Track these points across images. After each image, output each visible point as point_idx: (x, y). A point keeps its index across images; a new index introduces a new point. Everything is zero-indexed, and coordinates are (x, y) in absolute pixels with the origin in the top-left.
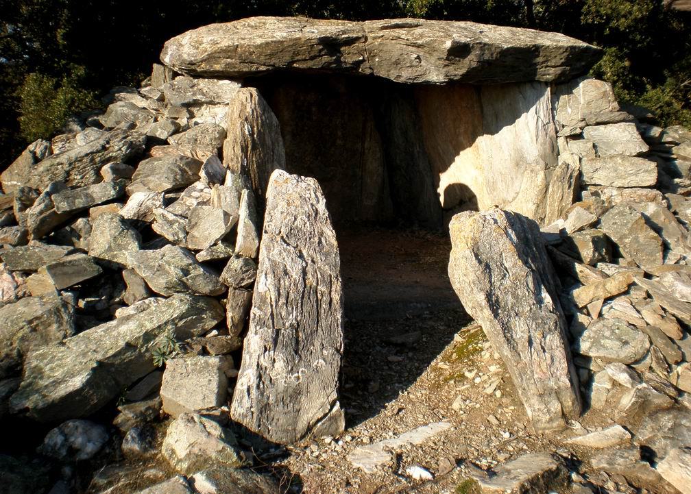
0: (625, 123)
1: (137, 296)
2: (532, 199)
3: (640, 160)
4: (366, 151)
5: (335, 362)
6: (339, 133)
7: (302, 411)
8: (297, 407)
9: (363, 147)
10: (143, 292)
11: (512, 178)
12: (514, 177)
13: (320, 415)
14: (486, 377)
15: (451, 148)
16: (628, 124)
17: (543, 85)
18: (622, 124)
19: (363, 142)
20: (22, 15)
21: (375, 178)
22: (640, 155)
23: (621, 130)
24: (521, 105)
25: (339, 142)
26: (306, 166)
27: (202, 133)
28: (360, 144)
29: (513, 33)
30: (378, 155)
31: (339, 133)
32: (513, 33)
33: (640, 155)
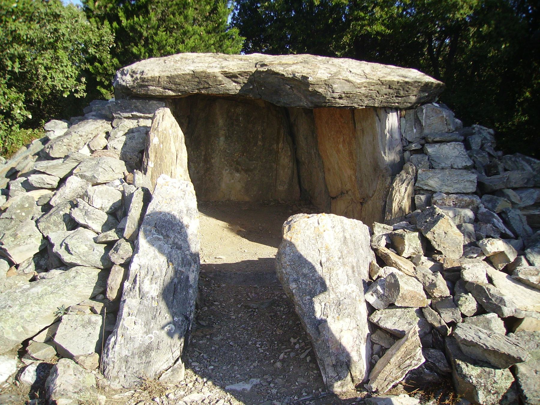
0: (454, 143)
1: (54, 265)
2: (382, 197)
3: (464, 172)
4: (280, 150)
5: (183, 327)
6: (260, 137)
7: (151, 363)
8: (148, 360)
9: (278, 147)
10: (57, 262)
11: (372, 180)
12: (373, 179)
13: (166, 367)
14: (303, 344)
15: (335, 152)
16: (457, 143)
17: (382, 112)
18: (453, 143)
19: (278, 144)
20: (268, 3)
21: (286, 170)
22: (466, 168)
23: (451, 148)
24: (377, 124)
25: (260, 143)
26: (235, 160)
27: (130, 139)
28: (275, 145)
29: (373, 69)
30: (290, 153)
31: (260, 137)
32: (373, 69)
33: (466, 168)
